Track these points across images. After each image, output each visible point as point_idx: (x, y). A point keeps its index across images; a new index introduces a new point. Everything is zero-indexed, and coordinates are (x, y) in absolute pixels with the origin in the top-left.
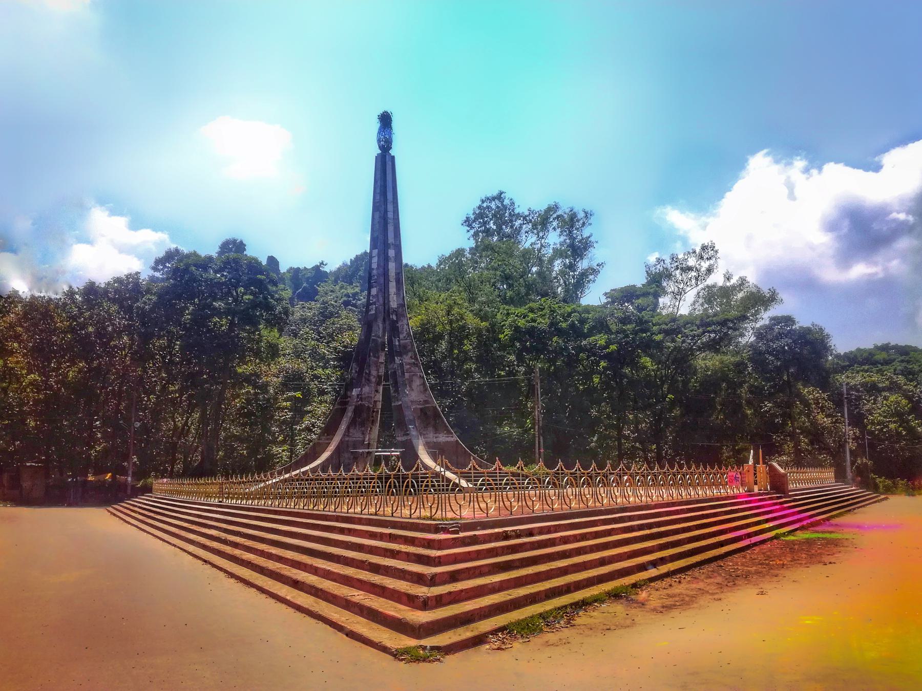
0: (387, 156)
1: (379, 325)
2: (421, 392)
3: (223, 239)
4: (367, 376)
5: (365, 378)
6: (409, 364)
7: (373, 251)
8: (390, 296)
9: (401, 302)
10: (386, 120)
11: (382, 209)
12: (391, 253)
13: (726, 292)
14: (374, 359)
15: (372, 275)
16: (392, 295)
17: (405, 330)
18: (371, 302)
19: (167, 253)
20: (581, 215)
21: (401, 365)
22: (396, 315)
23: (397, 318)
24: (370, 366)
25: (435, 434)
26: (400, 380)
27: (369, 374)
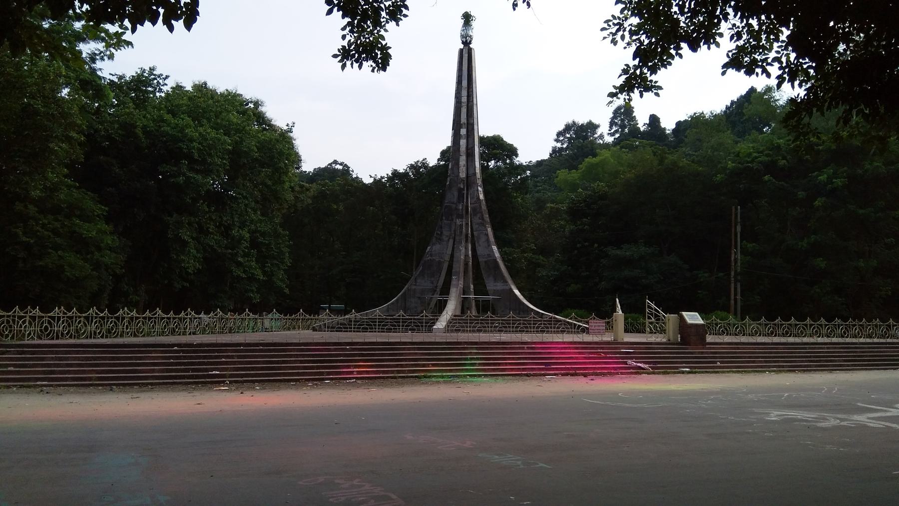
8: (460, 168)
10: (467, 18)
14: (447, 222)
17: (475, 195)
20: (626, 67)
24: (441, 228)
25: (495, 282)
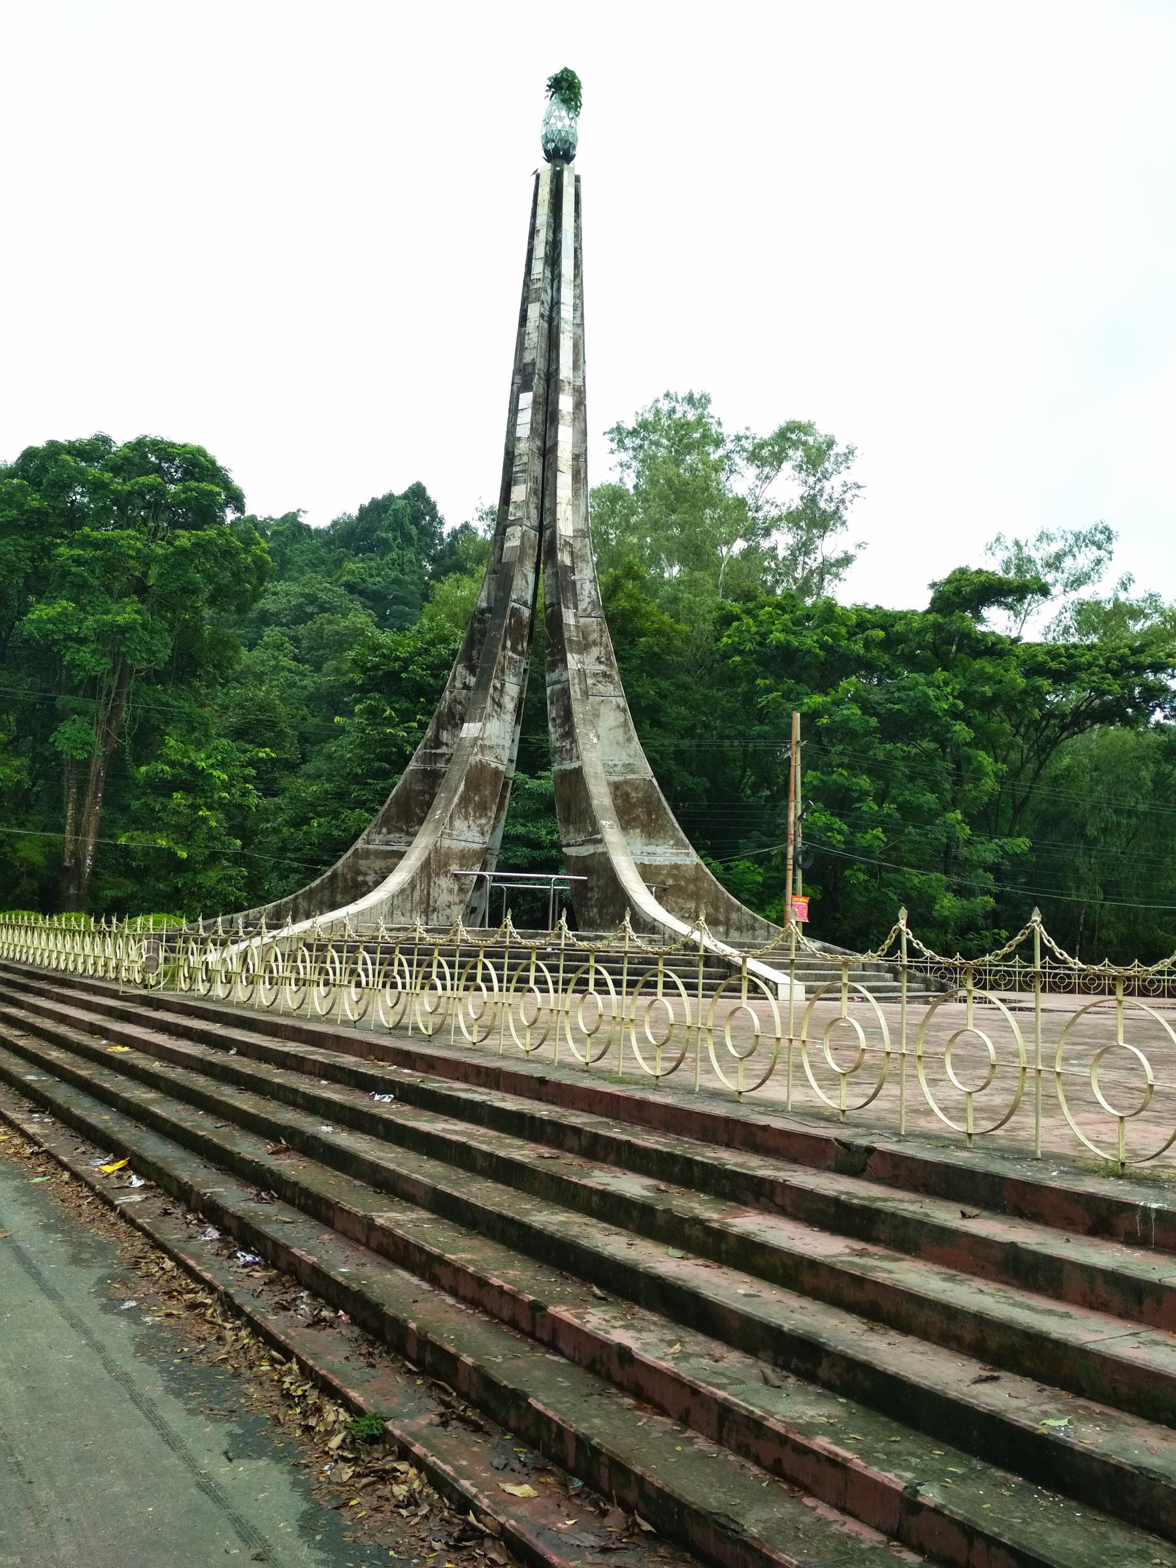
0: (566, 174)
1: (526, 576)
2: (618, 743)
4: (496, 696)
5: (493, 699)
6: (595, 675)
7: (522, 396)
8: (559, 508)
12: (566, 403)
13: (1123, 612)
15: (517, 452)
17: (586, 593)
21: (582, 674)
22: (572, 553)
23: (573, 561)
24: (503, 671)
26: (577, 708)
27: (502, 691)
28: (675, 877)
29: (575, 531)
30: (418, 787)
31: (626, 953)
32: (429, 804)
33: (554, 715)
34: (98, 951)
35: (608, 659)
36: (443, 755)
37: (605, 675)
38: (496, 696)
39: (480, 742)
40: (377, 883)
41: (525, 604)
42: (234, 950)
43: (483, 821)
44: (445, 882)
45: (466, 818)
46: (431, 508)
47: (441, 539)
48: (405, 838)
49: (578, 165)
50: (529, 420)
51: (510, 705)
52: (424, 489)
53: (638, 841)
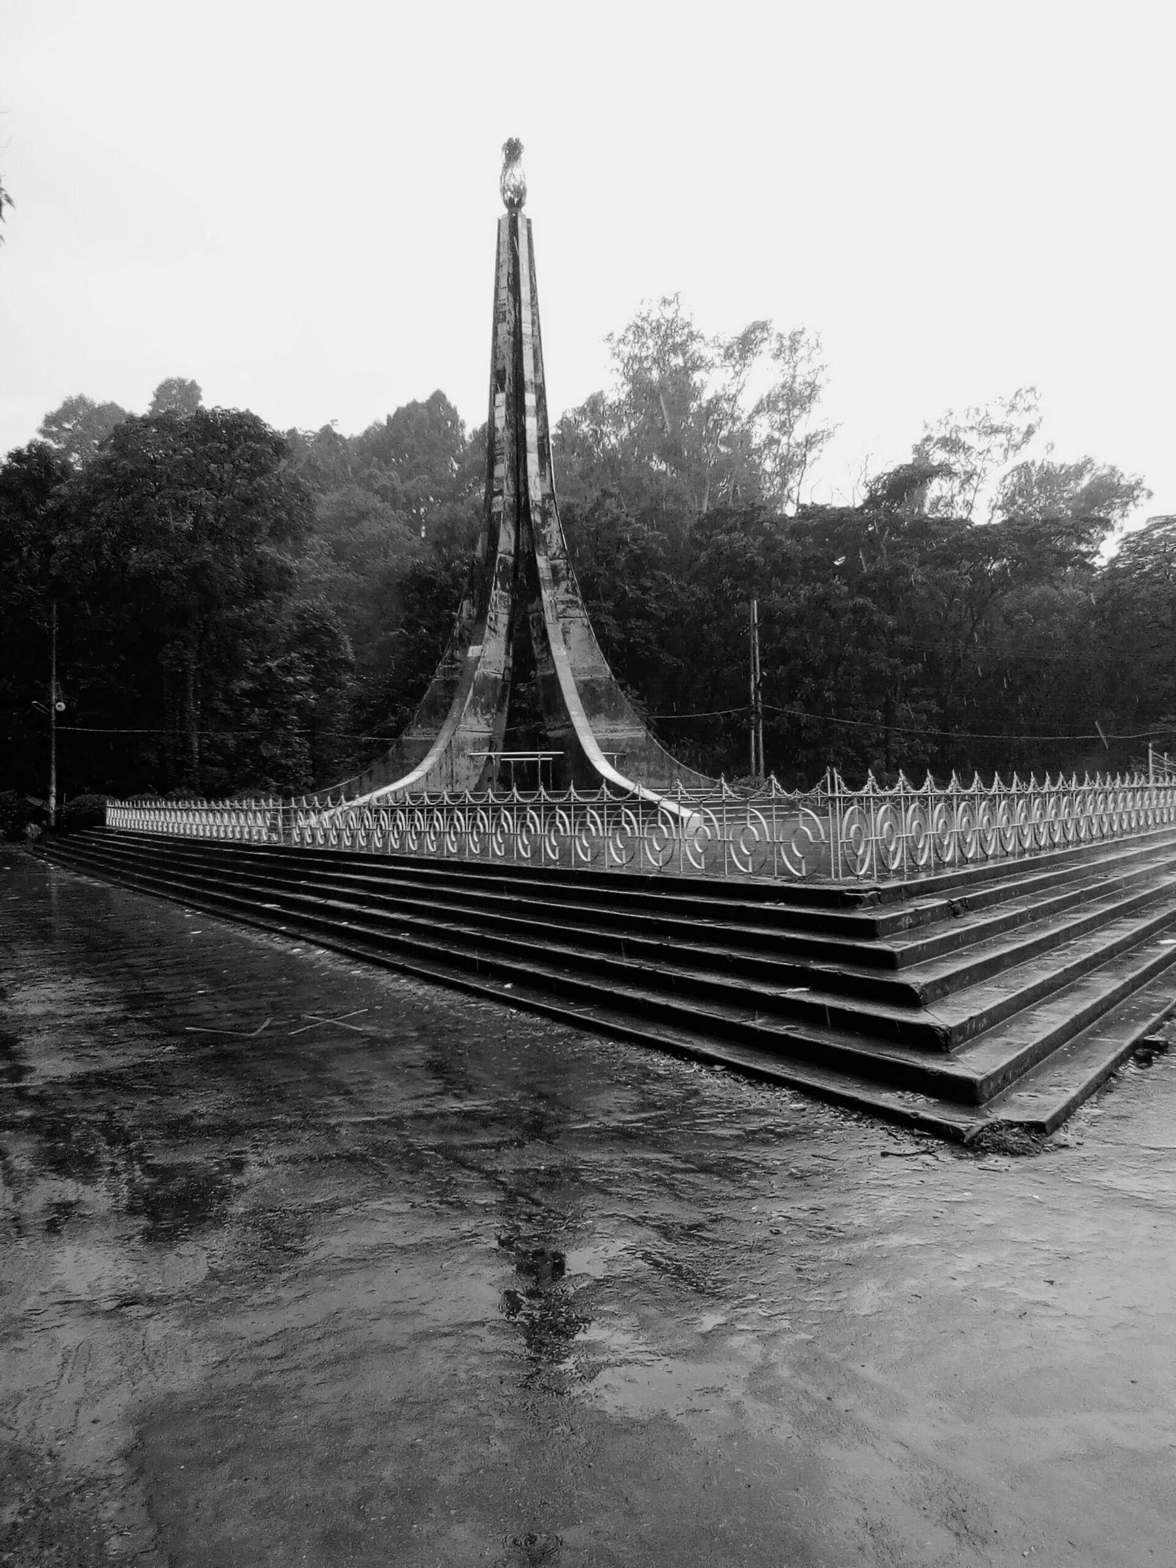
0: (520, 219)
3: (174, 375)
5: (490, 627)
9: (548, 491)
11: (510, 317)
12: (530, 399)
16: (533, 478)
18: (495, 490)
19: (65, 404)
28: (631, 747)
29: (543, 495)
30: (441, 693)
31: (605, 803)
32: (450, 705)
33: (535, 635)
34: (234, 822)
35: (574, 589)
36: (456, 669)
37: (572, 602)
38: (492, 624)
39: (482, 660)
40: (417, 764)
41: (509, 554)
42: (326, 815)
43: (488, 716)
44: (463, 762)
45: (475, 715)
46: (452, 413)
47: (464, 442)
48: (434, 731)
49: (526, 211)
50: (504, 414)
51: (503, 630)
52: (444, 396)
53: (603, 724)
